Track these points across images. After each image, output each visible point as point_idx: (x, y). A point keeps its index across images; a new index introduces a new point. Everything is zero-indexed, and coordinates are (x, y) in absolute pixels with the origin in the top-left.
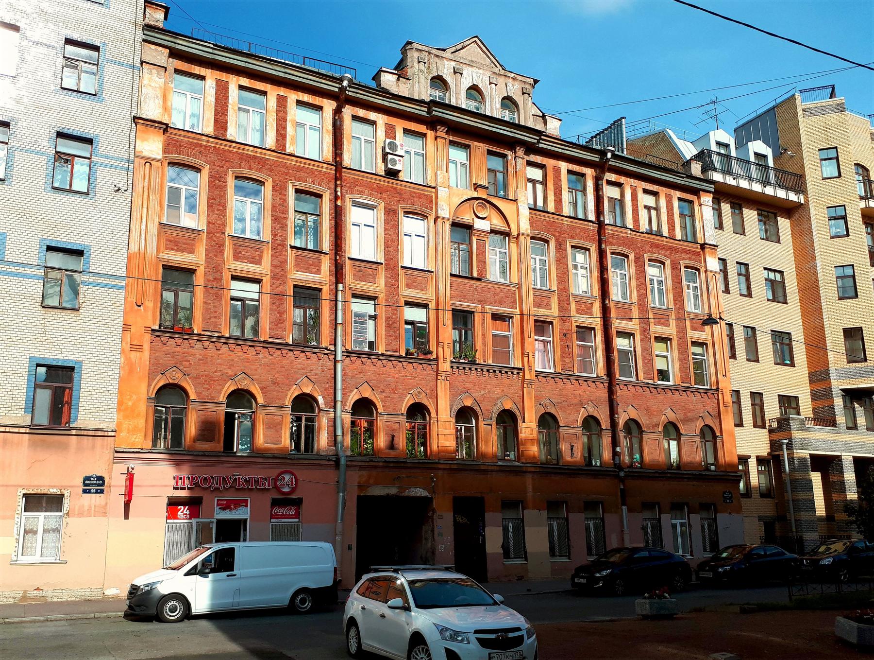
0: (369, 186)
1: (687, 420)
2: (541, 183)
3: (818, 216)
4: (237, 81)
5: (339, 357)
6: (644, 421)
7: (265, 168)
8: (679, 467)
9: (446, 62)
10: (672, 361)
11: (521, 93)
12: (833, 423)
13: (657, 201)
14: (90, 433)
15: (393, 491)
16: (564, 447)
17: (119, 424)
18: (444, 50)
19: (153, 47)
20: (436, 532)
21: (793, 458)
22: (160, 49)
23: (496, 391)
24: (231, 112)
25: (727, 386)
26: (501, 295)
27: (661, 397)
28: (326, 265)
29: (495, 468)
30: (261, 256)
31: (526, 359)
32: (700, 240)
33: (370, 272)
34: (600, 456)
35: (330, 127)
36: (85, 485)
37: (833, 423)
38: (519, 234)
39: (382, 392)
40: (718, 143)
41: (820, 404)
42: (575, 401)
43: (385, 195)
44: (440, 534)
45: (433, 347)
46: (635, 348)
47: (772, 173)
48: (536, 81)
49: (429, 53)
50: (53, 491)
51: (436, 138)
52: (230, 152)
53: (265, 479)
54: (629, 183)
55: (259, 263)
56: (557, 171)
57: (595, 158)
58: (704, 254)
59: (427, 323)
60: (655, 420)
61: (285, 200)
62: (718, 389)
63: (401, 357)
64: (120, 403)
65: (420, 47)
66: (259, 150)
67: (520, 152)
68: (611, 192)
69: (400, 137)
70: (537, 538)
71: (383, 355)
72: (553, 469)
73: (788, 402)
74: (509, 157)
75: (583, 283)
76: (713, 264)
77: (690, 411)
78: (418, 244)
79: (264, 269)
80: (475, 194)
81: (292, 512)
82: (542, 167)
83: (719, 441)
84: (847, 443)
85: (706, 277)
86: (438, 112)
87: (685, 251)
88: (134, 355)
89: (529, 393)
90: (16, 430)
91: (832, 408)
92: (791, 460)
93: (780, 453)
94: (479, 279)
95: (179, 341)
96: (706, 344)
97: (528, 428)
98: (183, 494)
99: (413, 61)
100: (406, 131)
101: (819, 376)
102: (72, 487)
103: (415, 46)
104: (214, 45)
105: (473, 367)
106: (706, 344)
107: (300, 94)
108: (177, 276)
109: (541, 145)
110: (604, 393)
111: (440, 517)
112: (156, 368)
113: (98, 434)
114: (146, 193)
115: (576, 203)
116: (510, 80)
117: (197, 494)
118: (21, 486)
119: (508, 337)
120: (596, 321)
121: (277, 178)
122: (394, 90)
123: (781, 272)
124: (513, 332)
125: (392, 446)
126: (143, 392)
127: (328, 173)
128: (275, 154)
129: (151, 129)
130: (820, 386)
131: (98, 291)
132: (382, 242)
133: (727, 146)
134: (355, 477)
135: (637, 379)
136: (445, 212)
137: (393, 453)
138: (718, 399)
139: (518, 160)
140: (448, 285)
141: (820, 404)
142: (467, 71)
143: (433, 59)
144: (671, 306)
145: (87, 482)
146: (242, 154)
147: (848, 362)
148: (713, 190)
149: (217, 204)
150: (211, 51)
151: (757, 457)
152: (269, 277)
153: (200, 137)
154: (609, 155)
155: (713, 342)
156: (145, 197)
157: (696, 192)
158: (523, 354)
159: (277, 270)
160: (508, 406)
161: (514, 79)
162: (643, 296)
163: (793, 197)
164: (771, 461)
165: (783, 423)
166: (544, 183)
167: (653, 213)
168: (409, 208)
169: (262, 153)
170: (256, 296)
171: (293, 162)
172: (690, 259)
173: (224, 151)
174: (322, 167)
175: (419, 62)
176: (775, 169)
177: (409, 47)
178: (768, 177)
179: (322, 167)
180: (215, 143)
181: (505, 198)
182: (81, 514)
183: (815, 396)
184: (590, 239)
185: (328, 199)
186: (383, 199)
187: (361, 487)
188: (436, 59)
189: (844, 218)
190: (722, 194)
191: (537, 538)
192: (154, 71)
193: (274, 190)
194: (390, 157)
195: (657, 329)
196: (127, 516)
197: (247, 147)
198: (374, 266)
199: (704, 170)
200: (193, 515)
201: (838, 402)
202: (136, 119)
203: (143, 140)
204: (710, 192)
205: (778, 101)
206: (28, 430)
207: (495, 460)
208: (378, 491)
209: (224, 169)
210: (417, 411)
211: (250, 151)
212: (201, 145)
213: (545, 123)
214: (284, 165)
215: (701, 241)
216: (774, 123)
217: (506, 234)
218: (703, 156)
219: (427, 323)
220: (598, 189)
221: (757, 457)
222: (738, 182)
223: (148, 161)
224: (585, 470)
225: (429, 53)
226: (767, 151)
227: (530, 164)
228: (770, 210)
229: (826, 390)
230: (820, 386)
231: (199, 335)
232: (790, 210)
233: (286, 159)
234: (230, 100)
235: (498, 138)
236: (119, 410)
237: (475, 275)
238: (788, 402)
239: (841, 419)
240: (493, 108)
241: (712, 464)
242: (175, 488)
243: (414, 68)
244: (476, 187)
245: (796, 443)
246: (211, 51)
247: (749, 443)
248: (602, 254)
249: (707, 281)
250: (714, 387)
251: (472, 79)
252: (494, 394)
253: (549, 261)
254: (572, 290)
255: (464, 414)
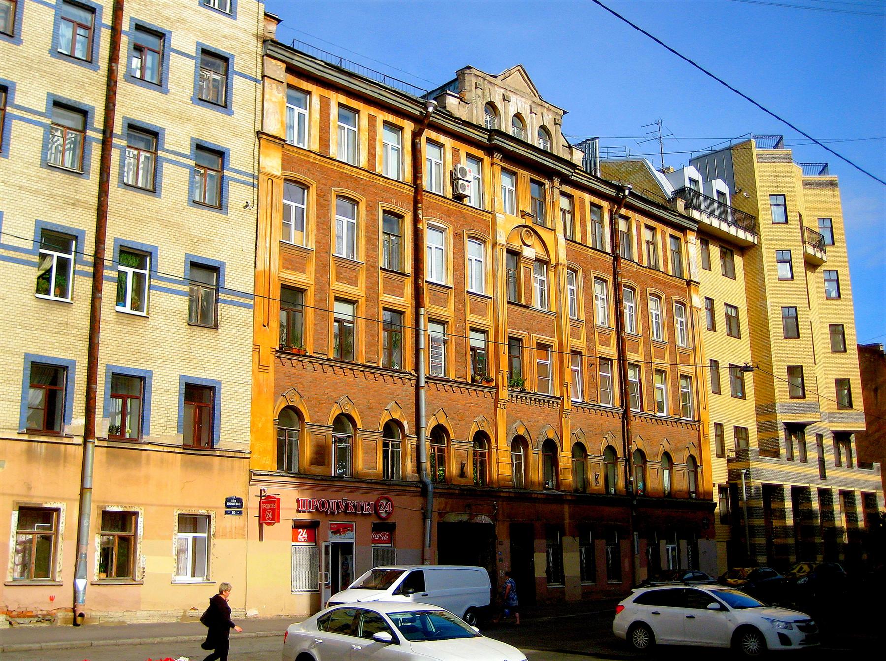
0: (440, 209)
1: (678, 450)
2: (569, 213)
3: (768, 256)
4: (337, 97)
5: (422, 383)
6: (647, 451)
7: (351, 186)
8: (670, 493)
9: (496, 89)
10: (667, 393)
11: (553, 123)
12: (776, 455)
13: (654, 236)
14: (231, 454)
15: (465, 518)
16: (591, 476)
17: (252, 446)
18: (496, 77)
19: (274, 61)
20: (498, 557)
21: (750, 487)
22: (279, 63)
23: (540, 420)
24: (332, 130)
25: (711, 418)
26: (543, 323)
27: (659, 427)
28: (409, 289)
29: (542, 496)
30: (357, 278)
31: (564, 389)
32: (686, 277)
33: (442, 296)
34: (615, 485)
35: (410, 149)
36: (227, 506)
37: (776, 455)
38: (557, 264)
39: (453, 419)
40: (690, 180)
41: (766, 435)
42: (599, 432)
43: (452, 219)
44: (501, 560)
45: (492, 375)
46: (640, 380)
47: (729, 211)
48: (565, 112)
49: (484, 79)
50: (202, 512)
51: (492, 164)
52: (332, 170)
53: (369, 504)
54: (635, 217)
55: (355, 284)
56: (582, 201)
57: (612, 192)
58: (690, 291)
59: (486, 349)
60: (655, 450)
61: (375, 221)
62: (699, 421)
63: (467, 383)
64: (253, 425)
65: (478, 73)
66: (355, 169)
67: (557, 182)
68: (622, 225)
69: (464, 163)
70: (572, 564)
71: (453, 381)
72: (582, 496)
73: (741, 432)
74: (547, 187)
75: (602, 315)
76: (697, 301)
77: (680, 441)
78: (481, 270)
79: (358, 291)
80: (523, 222)
81: (386, 538)
82: (570, 197)
83: (699, 470)
84: (787, 473)
85: (691, 313)
86: (498, 141)
87: (675, 286)
88: (262, 376)
89: (566, 423)
90: (172, 450)
91: (776, 441)
92: (749, 488)
93: (738, 482)
94: (527, 307)
95: (295, 362)
96: (690, 377)
97: (565, 457)
98: (305, 517)
99: (471, 85)
100: (469, 156)
101: (766, 409)
102: (216, 508)
103: (474, 71)
104: (326, 64)
105: (524, 396)
106: (690, 377)
107: (386, 114)
108: (291, 295)
109: (573, 177)
110: (618, 423)
111: (501, 544)
112: (279, 391)
113: (236, 455)
114: (269, 211)
115: (594, 231)
116: (545, 110)
117: (317, 518)
118: (176, 506)
119: (546, 365)
120: (611, 351)
121: (369, 198)
122: (457, 114)
123: (736, 308)
124: (551, 361)
125: (462, 474)
126: (271, 413)
127: (409, 195)
128: (367, 174)
129: (272, 144)
130: (765, 419)
131: (234, 310)
132: (451, 267)
133: (723, 195)
134: (436, 504)
135: (642, 410)
136: (502, 239)
137: (463, 481)
138: (699, 431)
139: (553, 188)
140: (506, 312)
141: (766, 435)
142: (513, 98)
143: (487, 85)
144: (666, 340)
145: (229, 503)
146: (342, 173)
147: (791, 398)
148: (696, 229)
149: (324, 225)
150: (321, 68)
151: (719, 485)
152: (364, 299)
153: (309, 154)
154: (627, 192)
155: (696, 376)
156: (269, 214)
157: (683, 229)
158: (561, 384)
159: (370, 291)
160: (551, 436)
161: (548, 109)
162: (647, 328)
163: (741, 234)
164: (731, 489)
165: (742, 454)
166: (572, 213)
167: (651, 246)
168: (472, 232)
169: (357, 173)
170: (351, 319)
171: (381, 182)
172: (679, 295)
173: (327, 168)
174: (403, 188)
175: (476, 87)
176: (733, 209)
177: (468, 71)
178: (726, 215)
179: (403, 188)
180: (321, 161)
181: (543, 225)
182: (224, 536)
183: (760, 428)
184: (607, 271)
185: (409, 221)
186: (451, 222)
187: (441, 514)
188: (489, 86)
189: (790, 262)
190: (707, 236)
191: (572, 564)
192: (274, 86)
193: (318, 195)
194: (460, 182)
195: (473, 318)
196: (261, 539)
197: (346, 166)
198: (445, 290)
199: (687, 207)
200: (311, 539)
201: (782, 434)
202: (259, 134)
203: (267, 156)
204: (693, 230)
205: (734, 142)
206: (181, 451)
207: (541, 488)
208: (453, 518)
209: (327, 188)
210: (481, 438)
211: (347, 170)
212: (308, 162)
213: (571, 154)
214: (374, 185)
215: (686, 277)
216: (728, 161)
217: (547, 263)
218: (681, 192)
219: (486, 349)
220: (613, 222)
221: (719, 485)
222: (711, 221)
223: (271, 177)
224: (606, 499)
225: (484, 79)
226: (725, 189)
227: (563, 194)
228: (731, 247)
229: (772, 422)
230: (765, 419)
231: (310, 356)
232: (743, 248)
233: (376, 179)
234: (332, 118)
235: (534, 166)
236: (251, 431)
237: (523, 302)
238: (741, 432)
239: (783, 451)
240: (533, 137)
241: (693, 492)
242: (298, 511)
243: (472, 94)
244: (524, 214)
245: (753, 473)
246: (321, 68)
247: (716, 473)
248: (617, 287)
249: (692, 317)
250: (696, 419)
251: (519, 109)
252: (540, 424)
253: (578, 291)
254: (334, 252)
255: (519, 442)
